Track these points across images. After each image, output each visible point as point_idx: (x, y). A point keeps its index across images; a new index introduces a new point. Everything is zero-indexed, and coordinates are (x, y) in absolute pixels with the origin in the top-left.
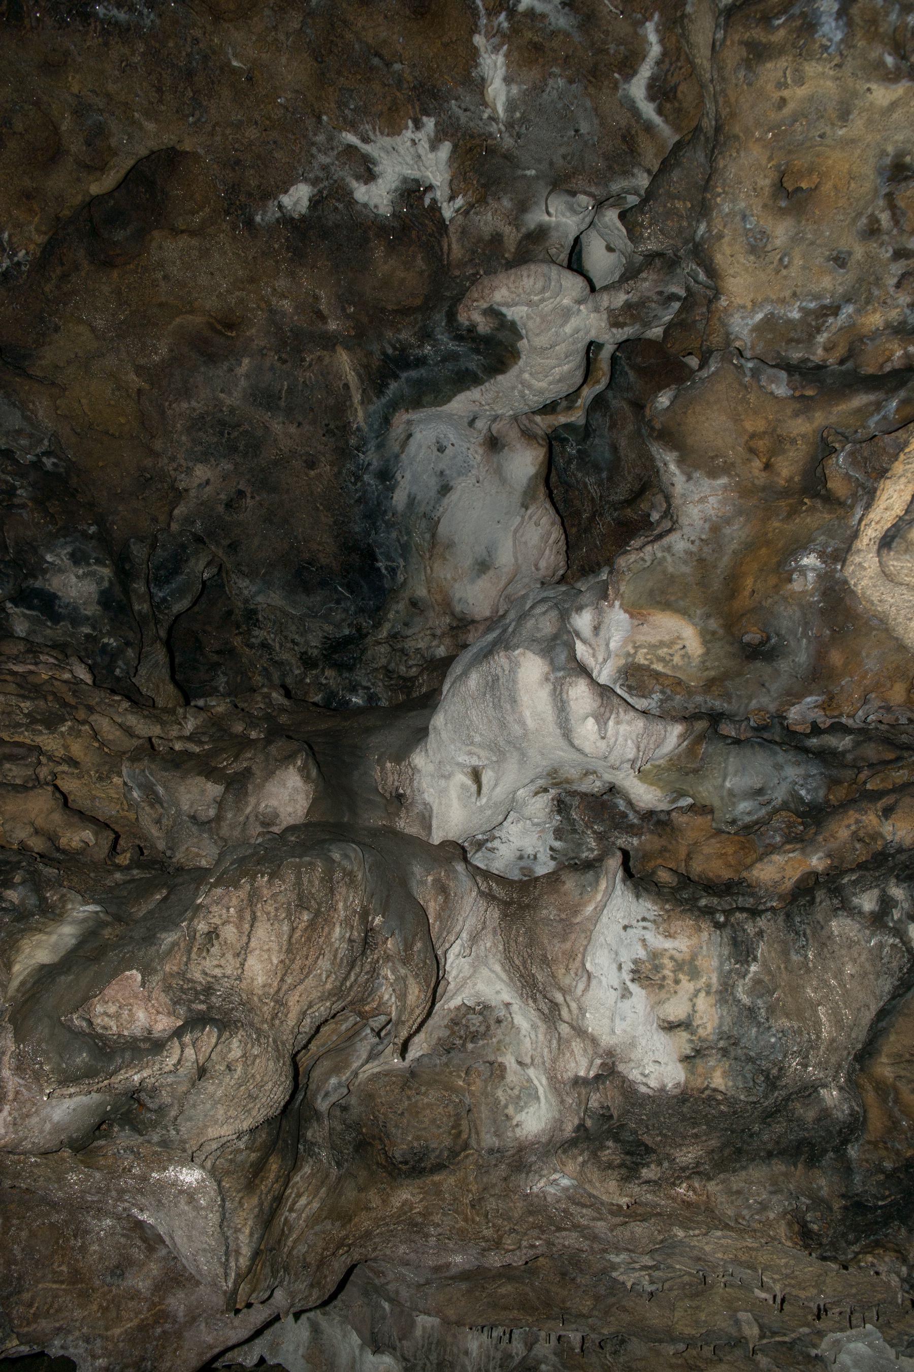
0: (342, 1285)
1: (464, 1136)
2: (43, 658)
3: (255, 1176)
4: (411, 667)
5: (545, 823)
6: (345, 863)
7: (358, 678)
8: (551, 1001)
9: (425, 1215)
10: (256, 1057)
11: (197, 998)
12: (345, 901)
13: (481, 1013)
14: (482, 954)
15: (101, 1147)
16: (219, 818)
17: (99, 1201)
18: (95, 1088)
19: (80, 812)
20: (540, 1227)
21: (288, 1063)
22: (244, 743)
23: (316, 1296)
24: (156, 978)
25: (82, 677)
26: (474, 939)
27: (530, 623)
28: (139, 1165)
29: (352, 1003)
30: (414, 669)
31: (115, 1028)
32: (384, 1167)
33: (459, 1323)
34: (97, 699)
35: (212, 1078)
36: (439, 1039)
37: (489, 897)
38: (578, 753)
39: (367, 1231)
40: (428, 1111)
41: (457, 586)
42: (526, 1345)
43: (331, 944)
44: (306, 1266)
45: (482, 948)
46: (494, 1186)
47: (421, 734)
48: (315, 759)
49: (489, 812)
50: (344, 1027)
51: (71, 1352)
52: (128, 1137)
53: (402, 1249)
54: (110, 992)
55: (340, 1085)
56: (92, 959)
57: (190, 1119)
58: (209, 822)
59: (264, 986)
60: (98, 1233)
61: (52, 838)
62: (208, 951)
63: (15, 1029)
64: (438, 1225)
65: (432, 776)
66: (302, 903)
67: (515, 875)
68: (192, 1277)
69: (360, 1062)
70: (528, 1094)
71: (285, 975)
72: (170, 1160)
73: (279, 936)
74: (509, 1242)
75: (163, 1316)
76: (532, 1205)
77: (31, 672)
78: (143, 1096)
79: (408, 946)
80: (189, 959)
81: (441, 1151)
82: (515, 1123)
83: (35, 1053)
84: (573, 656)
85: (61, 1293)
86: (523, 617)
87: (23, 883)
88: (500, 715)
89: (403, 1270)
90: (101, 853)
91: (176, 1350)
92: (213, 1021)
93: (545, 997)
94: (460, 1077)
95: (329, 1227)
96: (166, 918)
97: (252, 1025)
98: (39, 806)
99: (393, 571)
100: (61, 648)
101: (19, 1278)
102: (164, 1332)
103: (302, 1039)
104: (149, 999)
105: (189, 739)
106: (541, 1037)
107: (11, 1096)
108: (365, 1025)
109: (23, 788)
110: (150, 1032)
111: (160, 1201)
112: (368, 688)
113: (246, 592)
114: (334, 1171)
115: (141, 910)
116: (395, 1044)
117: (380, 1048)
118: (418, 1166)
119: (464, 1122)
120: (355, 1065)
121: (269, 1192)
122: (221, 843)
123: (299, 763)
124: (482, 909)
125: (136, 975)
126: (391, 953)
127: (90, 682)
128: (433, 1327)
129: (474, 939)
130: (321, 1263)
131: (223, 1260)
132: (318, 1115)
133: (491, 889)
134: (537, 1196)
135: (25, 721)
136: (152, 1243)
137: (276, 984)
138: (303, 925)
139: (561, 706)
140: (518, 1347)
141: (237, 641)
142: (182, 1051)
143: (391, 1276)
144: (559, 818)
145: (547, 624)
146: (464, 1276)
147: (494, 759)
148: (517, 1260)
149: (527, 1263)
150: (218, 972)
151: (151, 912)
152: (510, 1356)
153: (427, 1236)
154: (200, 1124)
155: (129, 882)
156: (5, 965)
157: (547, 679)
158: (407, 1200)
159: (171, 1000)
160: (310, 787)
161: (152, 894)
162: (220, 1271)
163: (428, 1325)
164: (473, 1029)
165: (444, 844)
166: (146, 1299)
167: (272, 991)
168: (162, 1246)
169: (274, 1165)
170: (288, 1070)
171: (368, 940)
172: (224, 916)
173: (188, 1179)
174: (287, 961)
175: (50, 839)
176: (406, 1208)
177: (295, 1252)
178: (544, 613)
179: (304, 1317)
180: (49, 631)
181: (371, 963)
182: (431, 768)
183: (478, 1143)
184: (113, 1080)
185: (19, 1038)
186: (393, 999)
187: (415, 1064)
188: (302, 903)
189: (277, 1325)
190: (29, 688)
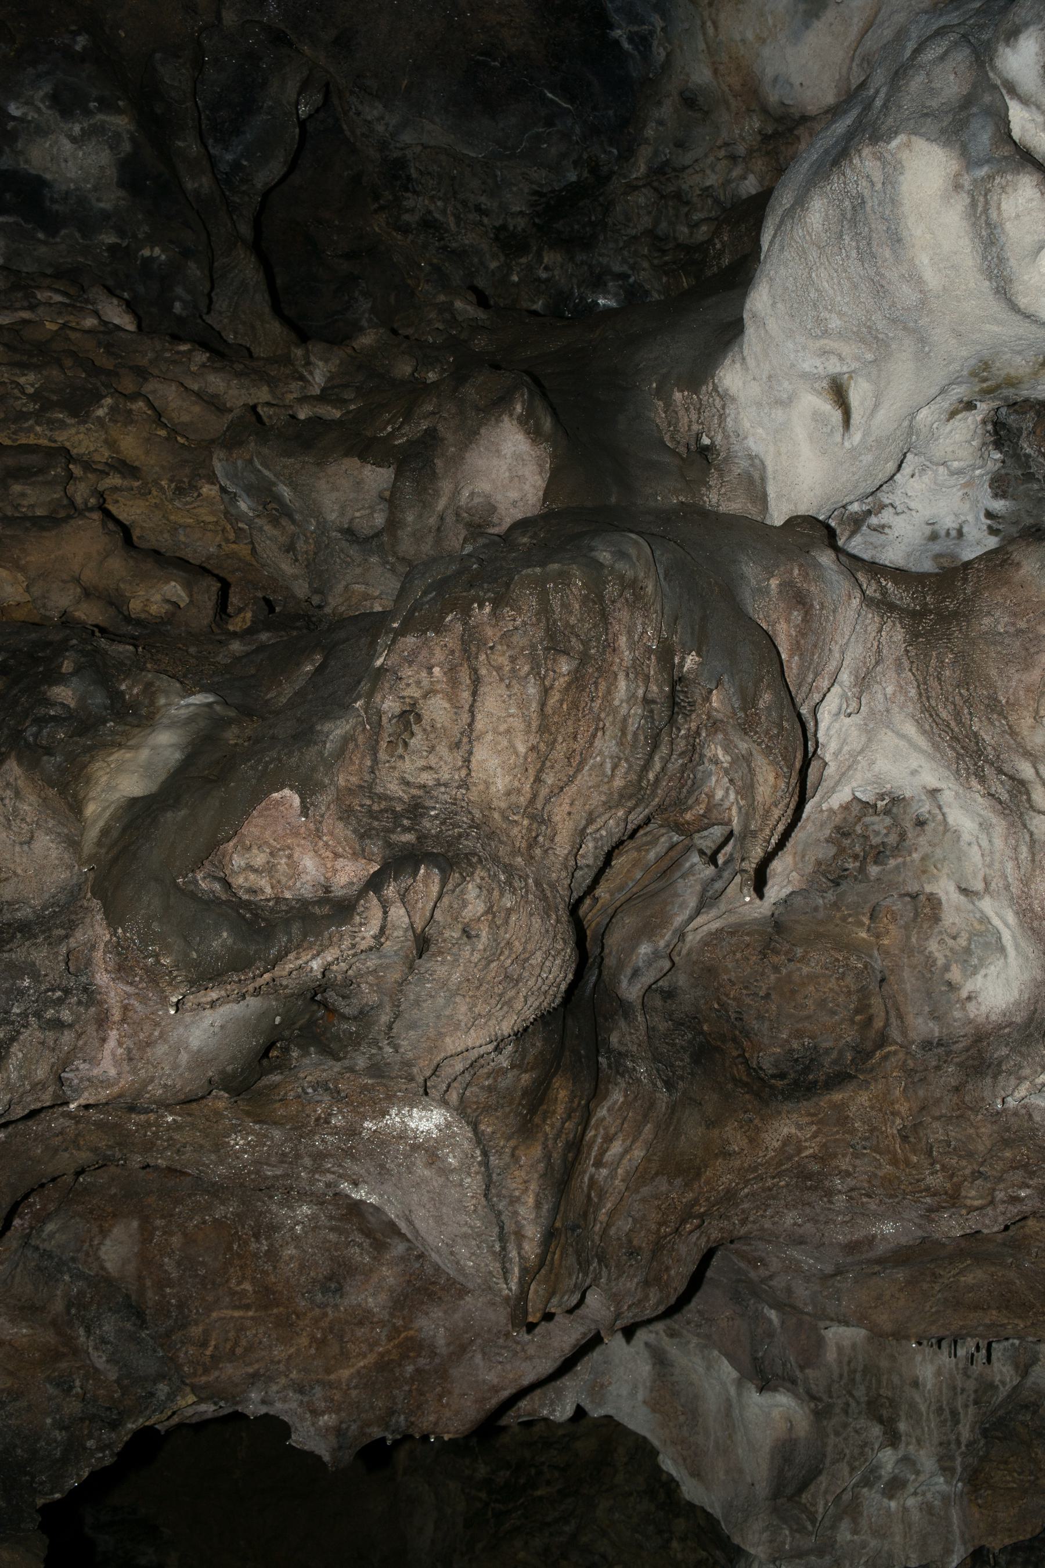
0: (696, 1282)
1: (878, 1023)
2: (41, 296)
3: (533, 1110)
4: (697, 225)
5: (974, 468)
6: (621, 566)
7: (604, 261)
8: (1011, 778)
9: (824, 1157)
10: (509, 911)
11: (397, 823)
12: (630, 633)
13: (887, 812)
14: (881, 707)
15: (276, 1086)
16: (393, 524)
17: (286, 1176)
18: (251, 988)
19: (156, 552)
20: (1025, 1166)
21: (565, 918)
22: (415, 392)
23: (654, 1301)
24: (324, 799)
25: (117, 321)
26: (864, 682)
27: (916, 83)
28: (340, 1111)
29: (662, 810)
30: (704, 228)
31: (268, 890)
32: (745, 1084)
33: (899, 1335)
34: (150, 355)
35: (440, 953)
36: (819, 863)
37: (883, 606)
38: (1026, 324)
39: (728, 1191)
40: (811, 988)
41: (766, 52)
42: (1017, 1367)
43: (615, 711)
44: (633, 1252)
45: (880, 696)
46: (938, 1101)
47: (730, 332)
48: (544, 395)
49: (868, 458)
50: (652, 855)
51: (278, 1408)
52: (316, 1065)
53: (790, 1218)
54: (251, 829)
55: (656, 955)
56: (214, 781)
57: (413, 1026)
58: (377, 535)
59: (508, 793)
60: (292, 1229)
61: (115, 602)
62: (406, 744)
63: (104, 905)
64: (848, 1174)
65: (759, 405)
66: (555, 643)
67: (928, 566)
68: (452, 1282)
69: (687, 913)
70: (985, 943)
71: (541, 770)
72: (390, 1098)
73: (523, 705)
74: (973, 1193)
75: (413, 1347)
76: (1008, 1130)
77: (25, 322)
78: (331, 996)
79: (748, 701)
80: (375, 761)
81: (841, 1053)
82: (964, 994)
83: (145, 941)
84: (1004, 133)
85: (248, 1323)
86: (899, 74)
87: (77, 671)
88: (872, 272)
89: (795, 1253)
90: (203, 616)
91: (440, 1397)
92: (430, 859)
93: (1000, 771)
94: (860, 924)
95: (664, 1187)
96: (329, 698)
97: (496, 859)
98: (82, 547)
99: (643, 42)
100: (72, 278)
101: (181, 1306)
102: (418, 1371)
103: (584, 877)
104: (318, 834)
105: (324, 397)
106: (999, 843)
107: (116, 1015)
108: (688, 849)
109: (51, 522)
110: (327, 890)
111: (382, 1166)
112: (624, 277)
113: (380, 128)
114: (663, 1096)
115: (283, 693)
116: (743, 871)
117: (718, 885)
118: (804, 1080)
119: (876, 1002)
120: (678, 921)
121: (558, 1136)
122: (403, 569)
123: (519, 408)
124: (872, 629)
125: (291, 797)
126: (720, 716)
127: (131, 327)
128: (854, 1346)
129: (864, 682)
130: (658, 1247)
131: (497, 1248)
132: (624, 1008)
133: (884, 591)
134: (1016, 1114)
135: (31, 407)
136: (379, 1236)
137: (527, 787)
138: (562, 682)
139: (988, 235)
140: (1002, 1372)
141: (378, 224)
142: (385, 913)
143: (775, 1264)
144: (998, 456)
145: (947, 79)
146: (902, 1257)
147: (869, 356)
148: (990, 1224)
149: (1007, 1228)
150: (426, 778)
151: (301, 694)
152: (991, 1387)
153: (830, 1193)
154: (432, 1033)
155: (257, 651)
156: (71, 807)
157: (957, 187)
158: (789, 1137)
159: (355, 831)
160: (544, 451)
161: (298, 665)
162: (495, 1266)
163: (846, 1343)
164: (875, 840)
165: (793, 522)
166: (382, 1323)
167: (523, 800)
168: (395, 1241)
169: (561, 1092)
170: (565, 929)
171: (677, 699)
172: (425, 683)
173: (424, 1126)
174: (542, 747)
175: (111, 603)
176: (791, 1149)
177: (612, 1231)
178: (942, 58)
179: (642, 1336)
180: (43, 249)
181: (686, 737)
182: (755, 390)
183: (904, 1033)
184: (278, 971)
185: (113, 920)
186: (732, 796)
187: (781, 909)
188: (555, 643)
189: (596, 1355)
190: (28, 349)
